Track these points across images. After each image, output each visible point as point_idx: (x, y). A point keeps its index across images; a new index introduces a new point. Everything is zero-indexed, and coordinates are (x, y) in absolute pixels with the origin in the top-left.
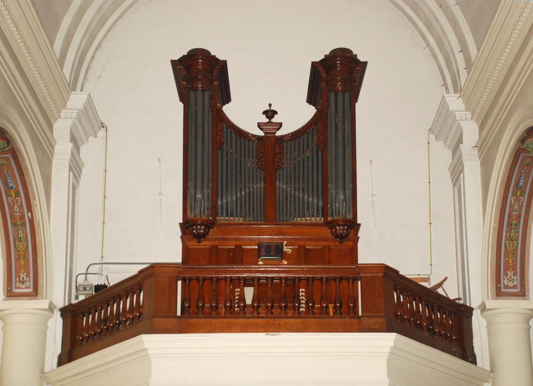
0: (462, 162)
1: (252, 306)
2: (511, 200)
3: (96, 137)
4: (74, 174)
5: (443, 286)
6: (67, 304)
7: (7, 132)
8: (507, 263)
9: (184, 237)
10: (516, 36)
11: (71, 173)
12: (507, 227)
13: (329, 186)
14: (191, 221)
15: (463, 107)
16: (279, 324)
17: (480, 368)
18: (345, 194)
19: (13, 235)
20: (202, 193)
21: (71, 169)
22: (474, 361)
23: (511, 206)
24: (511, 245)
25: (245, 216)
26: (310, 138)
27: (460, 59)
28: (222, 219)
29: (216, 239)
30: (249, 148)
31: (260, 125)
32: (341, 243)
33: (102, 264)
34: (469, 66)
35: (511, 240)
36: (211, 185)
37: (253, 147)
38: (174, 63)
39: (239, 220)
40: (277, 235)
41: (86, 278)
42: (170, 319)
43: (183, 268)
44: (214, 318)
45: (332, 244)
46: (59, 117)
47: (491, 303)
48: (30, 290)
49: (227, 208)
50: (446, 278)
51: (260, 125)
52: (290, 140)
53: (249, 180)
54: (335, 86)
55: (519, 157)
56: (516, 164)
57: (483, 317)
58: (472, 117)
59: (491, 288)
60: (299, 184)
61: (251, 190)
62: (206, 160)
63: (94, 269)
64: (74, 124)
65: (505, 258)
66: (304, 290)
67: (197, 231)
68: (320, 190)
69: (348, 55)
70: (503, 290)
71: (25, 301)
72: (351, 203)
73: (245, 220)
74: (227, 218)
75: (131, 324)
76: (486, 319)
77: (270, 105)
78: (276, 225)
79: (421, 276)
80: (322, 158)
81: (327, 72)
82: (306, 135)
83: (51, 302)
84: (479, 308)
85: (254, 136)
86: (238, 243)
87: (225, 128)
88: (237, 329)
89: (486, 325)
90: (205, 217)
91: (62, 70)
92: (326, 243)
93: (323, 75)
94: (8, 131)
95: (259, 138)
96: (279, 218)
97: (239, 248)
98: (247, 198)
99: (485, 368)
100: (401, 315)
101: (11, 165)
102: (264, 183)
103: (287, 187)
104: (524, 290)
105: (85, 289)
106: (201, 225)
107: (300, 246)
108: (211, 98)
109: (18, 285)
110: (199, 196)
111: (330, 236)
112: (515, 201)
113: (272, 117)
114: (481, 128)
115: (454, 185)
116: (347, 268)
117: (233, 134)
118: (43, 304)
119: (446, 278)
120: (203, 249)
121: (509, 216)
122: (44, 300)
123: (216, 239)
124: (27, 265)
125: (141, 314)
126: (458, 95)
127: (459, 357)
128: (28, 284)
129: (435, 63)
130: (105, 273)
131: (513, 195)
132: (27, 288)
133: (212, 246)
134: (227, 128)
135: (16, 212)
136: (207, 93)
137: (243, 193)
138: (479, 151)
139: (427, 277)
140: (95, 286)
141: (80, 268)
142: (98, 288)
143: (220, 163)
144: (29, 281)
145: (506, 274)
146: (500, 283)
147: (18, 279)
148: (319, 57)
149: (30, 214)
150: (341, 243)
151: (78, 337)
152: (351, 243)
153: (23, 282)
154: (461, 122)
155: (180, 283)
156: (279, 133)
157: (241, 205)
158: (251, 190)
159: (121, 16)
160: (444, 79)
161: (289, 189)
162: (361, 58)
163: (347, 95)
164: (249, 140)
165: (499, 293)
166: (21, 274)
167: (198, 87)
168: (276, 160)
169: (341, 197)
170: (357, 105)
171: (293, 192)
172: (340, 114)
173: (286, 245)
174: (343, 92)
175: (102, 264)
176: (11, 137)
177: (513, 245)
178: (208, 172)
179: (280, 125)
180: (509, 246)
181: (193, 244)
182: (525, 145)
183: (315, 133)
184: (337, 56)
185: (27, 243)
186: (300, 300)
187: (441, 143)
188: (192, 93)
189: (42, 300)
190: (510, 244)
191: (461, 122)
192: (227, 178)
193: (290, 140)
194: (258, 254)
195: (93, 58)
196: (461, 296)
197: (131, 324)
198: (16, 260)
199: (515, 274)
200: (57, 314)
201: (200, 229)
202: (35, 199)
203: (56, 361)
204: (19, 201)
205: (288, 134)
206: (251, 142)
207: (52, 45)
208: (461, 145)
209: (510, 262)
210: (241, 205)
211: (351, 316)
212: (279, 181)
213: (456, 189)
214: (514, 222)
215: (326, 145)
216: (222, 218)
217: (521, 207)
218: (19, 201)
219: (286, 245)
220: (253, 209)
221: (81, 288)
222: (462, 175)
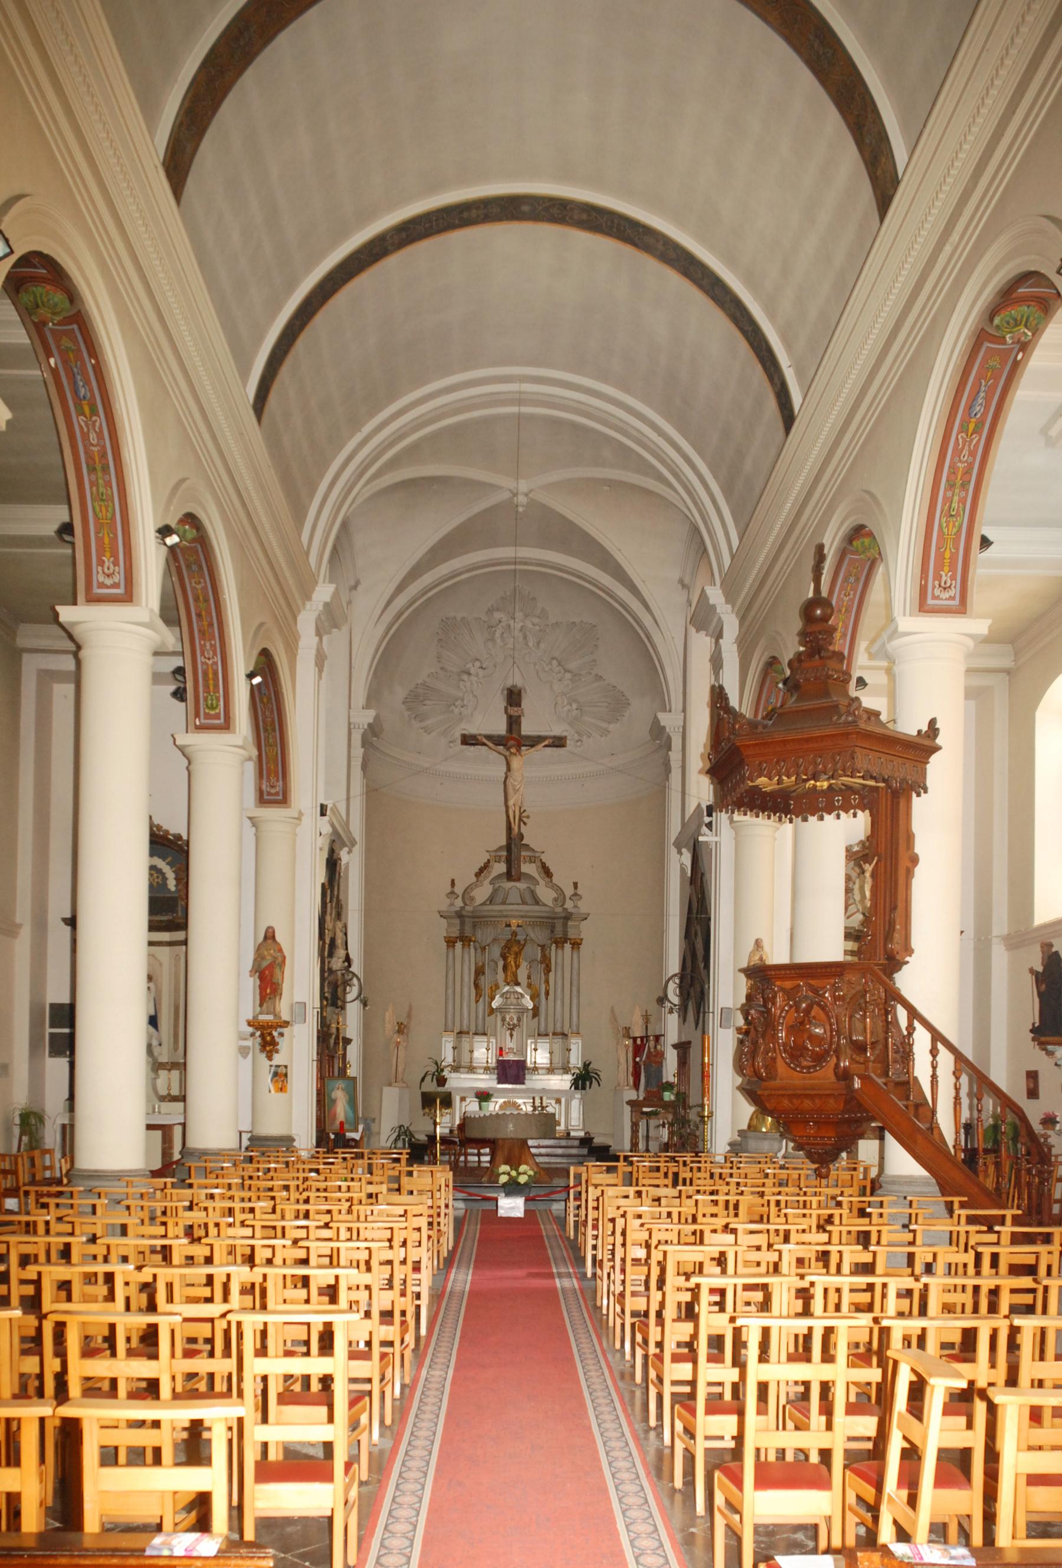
2: (957, 439)
8: (100, 541)
21: (316, 664)
24: (104, 509)
48: (120, 591)
94: (72, 276)
101: (79, 350)
114: (742, 620)
128: (952, 593)
135: (93, 445)
147: (937, 583)
165: (923, 607)
180: (947, 526)
190: (100, 506)
204: (974, 442)
209: (107, 541)
217: (100, 435)
218: (97, 424)
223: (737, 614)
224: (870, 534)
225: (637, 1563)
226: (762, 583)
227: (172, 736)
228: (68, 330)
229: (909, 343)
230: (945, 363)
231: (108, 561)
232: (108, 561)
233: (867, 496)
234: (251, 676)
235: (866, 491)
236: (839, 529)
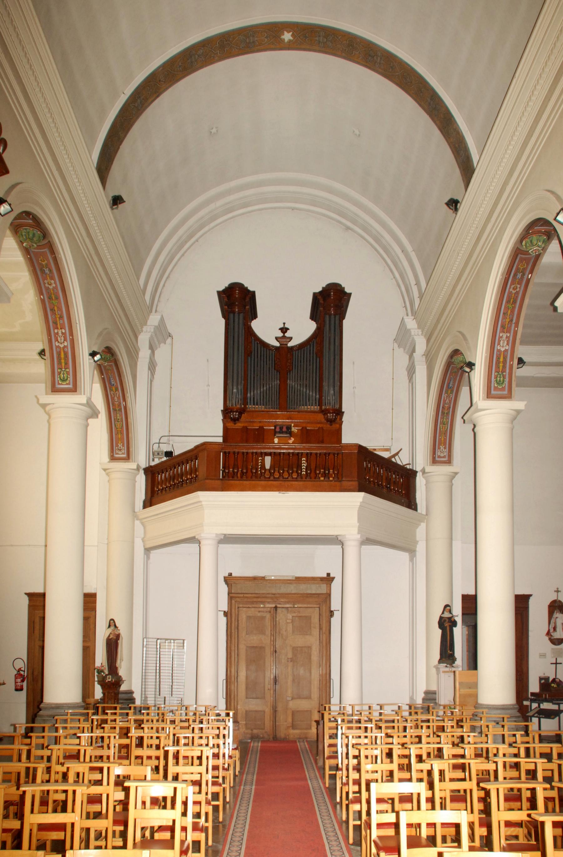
0: (414, 366)
1: (269, 470)
3: (165, 343)
4: (151, 372)
5: (399, 455)
6: (147, 466)
7: (112, 349)
8: (440, 440)
9: (225, 420)
10: (468, 241)
11: (149, 372)
12: (441, 415)
13: (324, 384)
14: (230, 409)
15: (416, 326)
16: (288, 485)
17: (419, 513)
18: (334, 390)
19: (114, 417)
20: (237, 389)
21: (149, 369)
22: (415, 509)
23: (444, 401)
25: (266, 405)
26: (312, 348)
27: (415, 290)
28: (250, 407)
29: (247, 422)
30: (269, 355)
31: (277, 338)
32: (331, 425)
33: (169, 436)
34: (421, 297)
35: (444, 424)
36: (243, 382)
37: (272, 354)
38: (219, 293)
39: (262, 408)
40: (288, 419)
41: (159, 446)
42: (216, 481)
43: (225, 445)
44: (245, 480)
45: (325, 426)
46: (142, 331)
47: (429, 469)
48: (125, 456)
49: (254, 398)
50: (401, 449)
51: (277, 338)
52: (298, 350)
53: (269, 379)
54: (330, 310)
55: (449, 367)
56: (448, 371)
57: (423, 477)
58: (422, 334)
59: (429, 458)
60: (303, 382)
61: (271, 386)
62: (240, 364)
63: (164, 440)
64: (152, 336)
65: (439, 437)
66: (305, 459)
67: (233, 416)
68: (318, 388)
69: (339, 288)
70: (437, 459)
71: (121, 463)
72: (338, 398)
73: (266, 408)
74: (254, 406)
75: (191, 482)
76: (425, 479)
77: (284, 324)
78: (287, 412)
79: (385, 447)
80: (319, 362)
81: (324, 300)
82: (308, 347)
83: (138, 464)
84: (421, 471)
85: (273, 346)
86: (261, 425)
87: (253, 341)
88: (260, 488)
89: (425, 483)
90: (238, 406)
91: (138, 281)
92: (319, 425)
93: (321, 301)
94: (113, 348)
95: (277, 348)
96: (289, 407)
97: (261, 429)
98: (268, 392)
99: (423, 513)
100: (368, 479)
101: (113, 369)
102: (280, 381)
103: (295, 384)
104: (450, 459)
105: (158, 454)
106: (236, 412)
107: (303, 428)
108: (244, 318)
109: (117, 452)
110: (235, 390)
111: (323, 420)
112: (447, 397)
113: (286, 332)
114: (428, 341)
115: (409, 382)
116: (334, 446)
117: (259, 345)
118: (133, 466)
119: (401, 449)
120: (237, 429)
121: (443, 407)
122: (134, 463)
123: (247, 422)
124: (122, 439)
125: (197, 476)
126: (413, 317)
127: (406, 507)
128: (123, 452)
129: (399, 290)
130: (171, 443)
131: (446, 393)
132: (123, 454)
133: (243, 427)
134: (255, 340)
136: (241, 315)
137: (265, 388)
138: (426, 358)
139: (389, 447)
140: (165, 452)
141: (155, 439)
142: (169, 454)
143: (249, 366)
144: (124, 449)
145: (439, 448)
146: (435, 454)
147: (117, 448)
148: (318, 289)
149: (124, 403)
150: (331, 425)
151: (155, 489)
152: (338, 426)
153: (120, 450)
154: (414, 336)
155: (222, 453)
156: (290, 344)
157: (263, 396)
158: (271, 386)
159: (183, 255)
160: (405, 302)
161: (296, 386)
162: (347, 290)
163: (337, 317)
164: (270, 350)
165: (434, 461)
166: (119, 444)
167: (235, 311)
168: (288, 364)
169: (332, 392)
170: (345, 322)
171: (299, 388)
172: (332, 332)
173: (293, 427)
174: (335, 315)
175: (169, 436)
176: (115, 352)
177: (445, 428)
178: (241, 374)
179: (291, 338)
181: (231, 425)
182: (453, 360)
183: (315, 344)
184: (331, 289)
185: (123, 423)
186: (302, 469)
187: (402, 349)
188: (232, 315)
189: (132, 463)
191: (414, 336)
192: (254, 378)
193: (298, 350)
194: (275, 432)
195: (164, 285)
196: (411, 463)
197: (191, 482)
198: (116, 434)
199: (445, 448)
200: (142, 472)
201: (236, 415)
202: (127, 392)
203: (142, 504)
204: (118, 394)
205: (297, 345)
206: (271, 351)
207: (138, 279)
208: (414, 354)
209: (443, 439)
210: (263, 396)
211: (335, 480)
212: (290, 380)
213: (411, 385)
214: (446, 412)
215: (322, 353)
216: (250, 406)
217: (119, 398)
218: (118, 394)
219: (293, 427)
220: (272, 400)
221: (156, 454)
222: (414, 375)
223: (425, 336)
224: (462, 354)
225: (331, 854)
226: (438, 321)
227: (36, 397)
228: (43, 252)
229: (471, 273)
230: (497, 270)
231: (120, 445)
232: (120, 445)
233: (460, 336)
234: (93, 354)
235: (459, 332)
236: (444, 356)
